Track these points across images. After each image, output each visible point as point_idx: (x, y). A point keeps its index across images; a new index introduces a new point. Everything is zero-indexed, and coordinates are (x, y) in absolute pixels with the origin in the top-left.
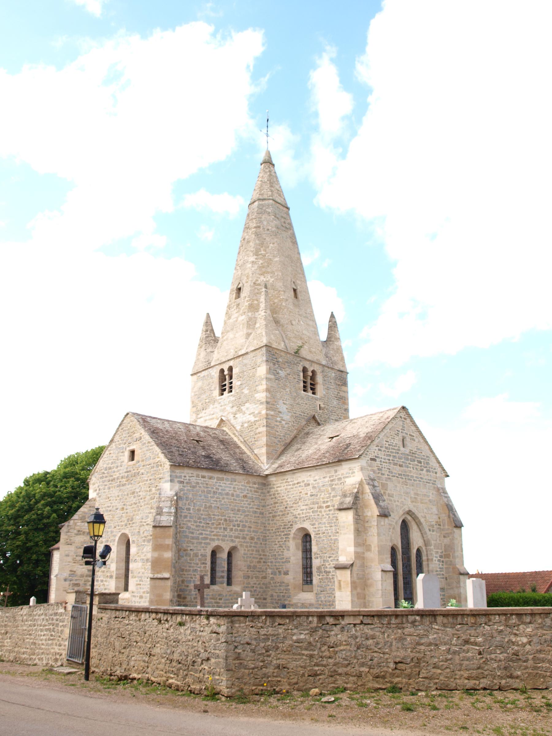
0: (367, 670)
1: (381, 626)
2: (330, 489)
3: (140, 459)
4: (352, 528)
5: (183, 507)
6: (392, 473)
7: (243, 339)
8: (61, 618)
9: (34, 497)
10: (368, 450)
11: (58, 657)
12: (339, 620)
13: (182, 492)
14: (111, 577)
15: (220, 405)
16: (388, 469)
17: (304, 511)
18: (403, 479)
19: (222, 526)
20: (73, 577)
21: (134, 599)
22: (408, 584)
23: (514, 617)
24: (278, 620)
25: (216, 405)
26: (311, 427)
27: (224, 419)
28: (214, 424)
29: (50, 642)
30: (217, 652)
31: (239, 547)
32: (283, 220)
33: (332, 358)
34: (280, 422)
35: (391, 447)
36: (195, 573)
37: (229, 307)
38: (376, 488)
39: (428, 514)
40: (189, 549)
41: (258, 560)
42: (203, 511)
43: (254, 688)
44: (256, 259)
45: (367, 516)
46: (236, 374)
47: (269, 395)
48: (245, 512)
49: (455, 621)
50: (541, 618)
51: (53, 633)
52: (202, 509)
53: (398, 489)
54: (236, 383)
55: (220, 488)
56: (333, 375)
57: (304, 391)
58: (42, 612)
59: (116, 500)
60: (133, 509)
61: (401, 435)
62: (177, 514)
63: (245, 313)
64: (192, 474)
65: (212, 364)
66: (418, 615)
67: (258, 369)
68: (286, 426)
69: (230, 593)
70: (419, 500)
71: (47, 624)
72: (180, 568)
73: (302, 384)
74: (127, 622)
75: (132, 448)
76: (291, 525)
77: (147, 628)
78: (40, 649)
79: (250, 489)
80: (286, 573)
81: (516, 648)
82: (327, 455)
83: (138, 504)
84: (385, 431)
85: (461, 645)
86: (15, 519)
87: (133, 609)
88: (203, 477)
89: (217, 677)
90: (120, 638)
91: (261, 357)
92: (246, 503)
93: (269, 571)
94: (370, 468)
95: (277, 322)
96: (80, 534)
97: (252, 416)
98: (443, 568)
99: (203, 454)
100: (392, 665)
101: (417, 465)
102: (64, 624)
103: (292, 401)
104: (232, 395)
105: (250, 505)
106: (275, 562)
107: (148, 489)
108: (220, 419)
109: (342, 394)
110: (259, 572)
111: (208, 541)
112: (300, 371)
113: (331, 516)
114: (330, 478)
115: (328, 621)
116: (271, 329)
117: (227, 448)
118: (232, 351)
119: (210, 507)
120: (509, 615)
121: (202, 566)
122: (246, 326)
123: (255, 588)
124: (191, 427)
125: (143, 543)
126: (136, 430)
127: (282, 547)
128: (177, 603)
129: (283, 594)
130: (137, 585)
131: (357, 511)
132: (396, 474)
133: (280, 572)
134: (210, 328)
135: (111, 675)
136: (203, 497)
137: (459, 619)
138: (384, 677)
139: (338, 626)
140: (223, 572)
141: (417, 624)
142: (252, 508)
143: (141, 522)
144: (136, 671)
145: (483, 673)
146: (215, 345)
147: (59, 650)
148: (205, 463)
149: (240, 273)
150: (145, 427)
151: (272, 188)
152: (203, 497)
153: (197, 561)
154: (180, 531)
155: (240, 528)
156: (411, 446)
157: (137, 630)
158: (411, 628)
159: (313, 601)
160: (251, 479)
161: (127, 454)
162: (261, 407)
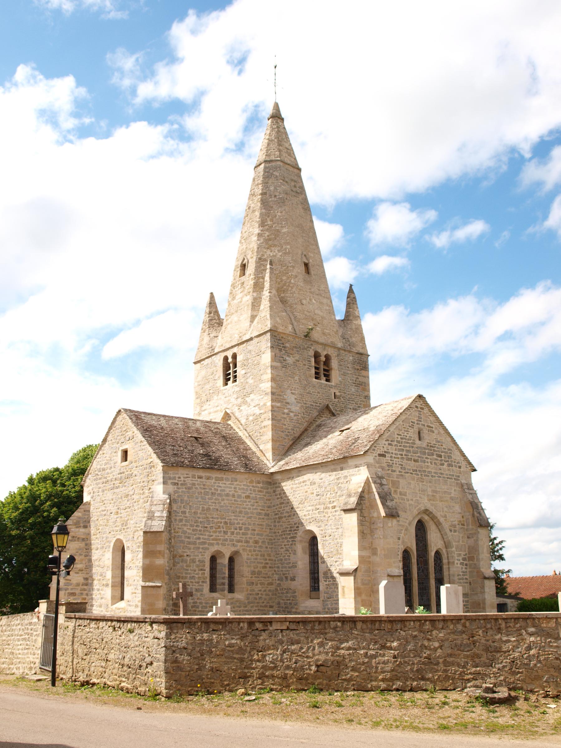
0: (292, 672)
1: (305, 631)
2: (336, 488)
3: (133, 461)
4: (356, 530)
5: (178, 510)
6: (405, 469)
7: (249, 324)
8: (35, 627)
9: (40, 497)
10: (375, 445)
11: (32, 665)
12: (267, 626)
13: (176, 495)
14: (107, 585)
15: (225, 396)
16: (399, 465)
17: (310, 512)
18: (418, 475)
19: (222, 530)
20: (68, 586)
21: (129, 608)
22: (425, 590)
23: (427, 623)
24: (212, 626)
25: (221, 396)
26: (324, 418)
27: (228, 411)
28: (218, 418)
29: (26, 651)
30: (158, 656)
31: (241, 552)
32: (293, 184)
33: (350, 339)
34: (288, 414)
35: (404, 440)
36: (192, 580)
37: (233, 286)
38: (384, 487)
39: (450, 513)
40: (185, 554)
41: (263, 565)
42: (200, 513)
43: (190, 689)
44: (262, 231)
45: (373, 517)
46: (240, 362)
47: (274, 385)
48: (247, 513)
49: (373, 628)
50: (453, 623)
51: (28, 643)
52: (199, 512)
53: (412, 486)
54: (240, 371)
55: (219, 489)
56: (351, 358)
57: (316, 378)
58: (18, 622)
59: (110, 503)
60: (128, 513)
61: (416, 426)
62: (170, 518)
63: (249, 292)
64: (187, 474)
65: (216, 351)
66: (339, 621)
67: (263, 356)
68: (295, 418)
69: (232, 601)
70: (438, 497)
71: (23, 633)
72: (176, 575)
73: (313, 371)
74: (88, 630)
75: (124, 447)
76: (298, 527)
77: (104, 635)
78: (17, 658)
79: (253, 488)
80: (293, 579)
81: (428, 652)
82: (334, 451)
83: (131, 508)
84: (397, 423)
85: (378, 649)
86: (19, 522)
87: (93, 618)
88: (200, 477)
89: (158, 679)
90: (83, 646)
91: (266, 342)
92: (249, 504)
93: (276, 577)
94: (377, 465)
95: (283, 301)
96: (75, 541)
97: (257, 408)
98: (466, 572)
99: (201, 452)
100: (314, 668)
101: (437, 460)
102: (38, 633)
103: (302, 391)
104: (236, 386)
105: (253, 506)
106: (282, 568)
107: (142, 492)
108: (224, 411)
109: (361, 379)
110: (265, 578)
111: (206, 546)
112: (311, 356)
113: (337, 517)
114: (336, 476)
115: (258, 627)
116: (276, 310)
117: (229, 444)
118: (236, 335)
119: (209, 509)
120: (423, 622)
121: (200, 572)
122: (250, 307)
123: (260, 596)
124: (191, 423)
125: (137, 550)
126: (129, 429)
127: (288, 551)
128: (173, 612)
129: (291, 601)
130: (133, 593)
131: (361, 512)
132: (410, 470)
133: (286, 578)
134: (214, 310)
135: (75, 681)
136: (200, 499)
137: (377, 624)
138: (307, 679)
139: (266, 632)
140: (224, 578)
141: (338, 629)
142: (255, 509)
143: (136, 527)
144: (95, 676)
145: (396, 675)
146: (219, 328)
147: (33, 658)
148: (202, 462)
149: (244, 247)
150: (137, 425)
151: (281, 148)
152: (200, 499)
153: (195, 568)
154: (175, 536)
155: (243, 531)
156: (428, 438)
157: (96, 637)
158: (333, 633)
159: (320, 609)
160: (254, 478)
161: (120, 454)
162: (266, 398)
